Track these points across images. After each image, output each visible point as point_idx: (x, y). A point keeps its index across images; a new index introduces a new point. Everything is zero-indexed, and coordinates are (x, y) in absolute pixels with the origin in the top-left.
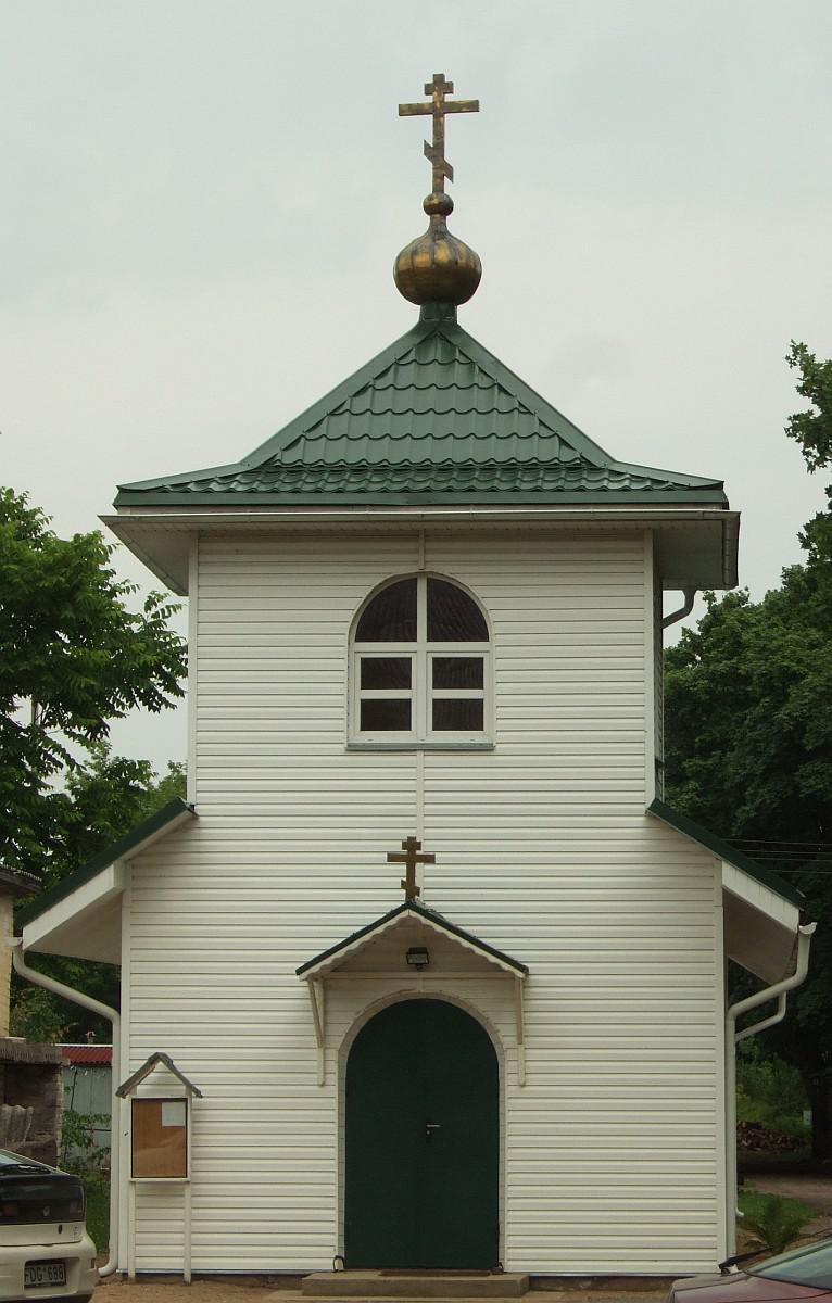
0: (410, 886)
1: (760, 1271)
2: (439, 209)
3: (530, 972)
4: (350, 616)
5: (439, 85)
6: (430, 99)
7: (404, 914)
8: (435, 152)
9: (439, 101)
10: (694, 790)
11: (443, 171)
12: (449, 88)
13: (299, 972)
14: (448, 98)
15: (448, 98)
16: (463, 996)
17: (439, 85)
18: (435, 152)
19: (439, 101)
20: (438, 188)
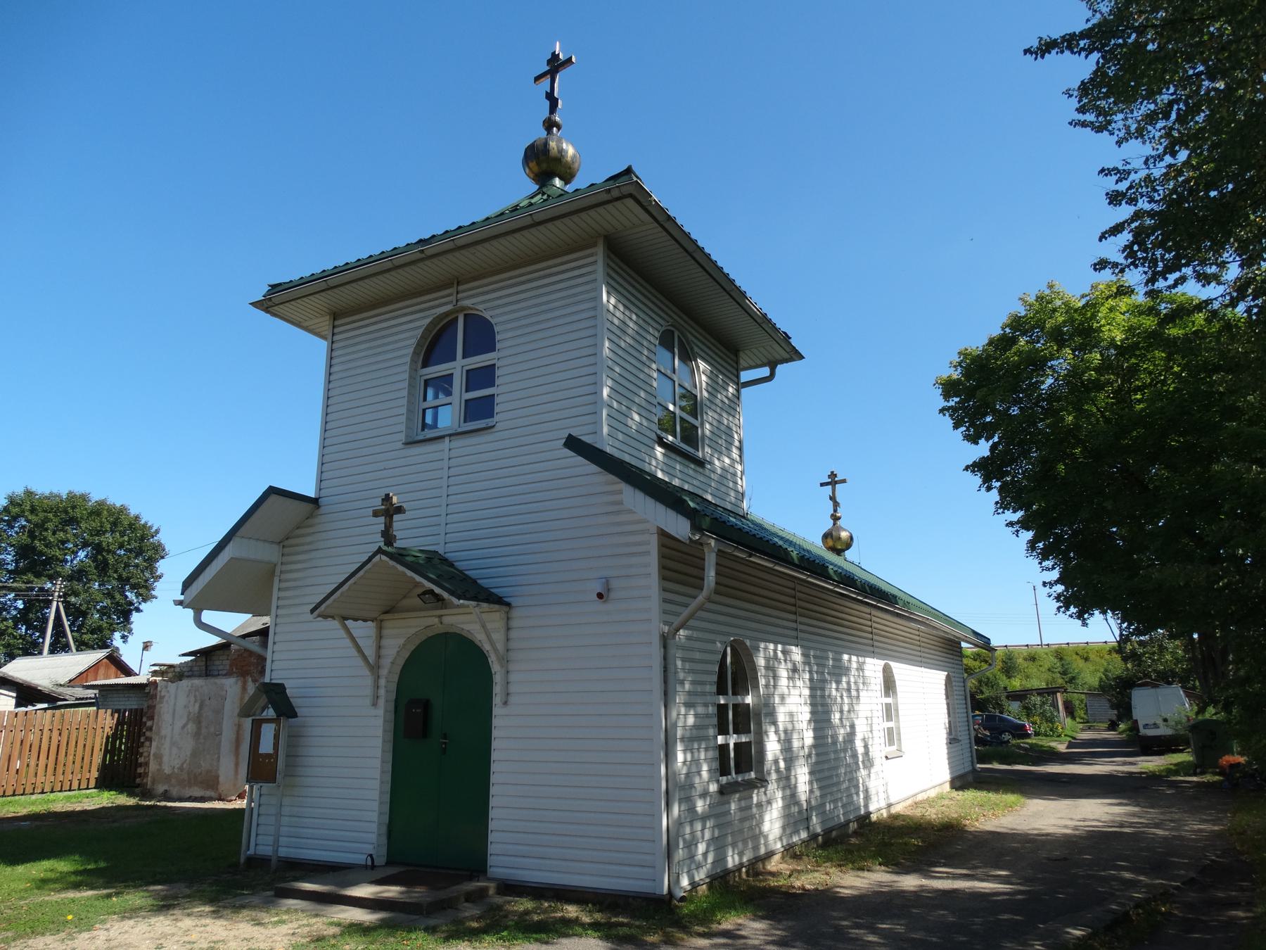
0: (388, 536)
1: (694, 343)
2: (835, 518)
3: (513, 604)
4: (414, 341)
5: (833, 475)
6: (830, 480)
7: (377, 558)
8: (833, 498)
9: (833, 481)
10: (1128, 312)
11: (836, 505)
12: (836, 475)
13: (312, 611)
14: (836, 479)
15: (836, 479)
16: (466, 627)
17: (833, 475)
18: (833, 498)
19: (833, 481)
20: (835, 511)
